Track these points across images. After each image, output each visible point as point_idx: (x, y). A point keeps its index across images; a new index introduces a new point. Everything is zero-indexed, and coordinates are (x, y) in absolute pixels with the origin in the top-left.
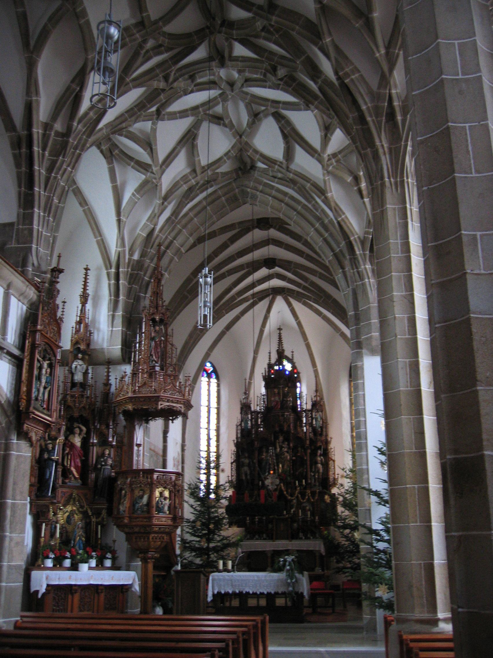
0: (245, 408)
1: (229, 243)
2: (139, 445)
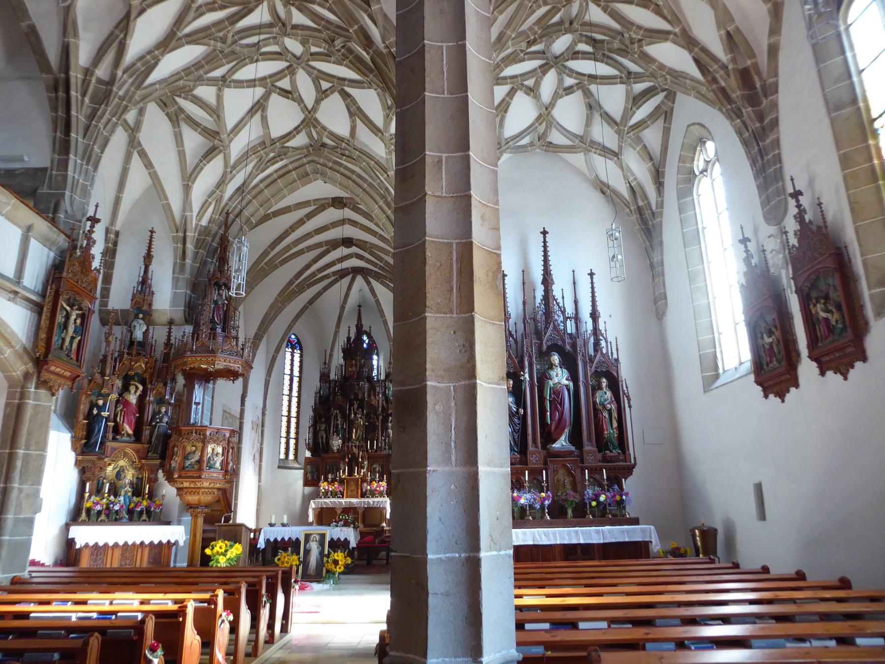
0: (324, 377)
1: (305, 219)
2: (197, 404)
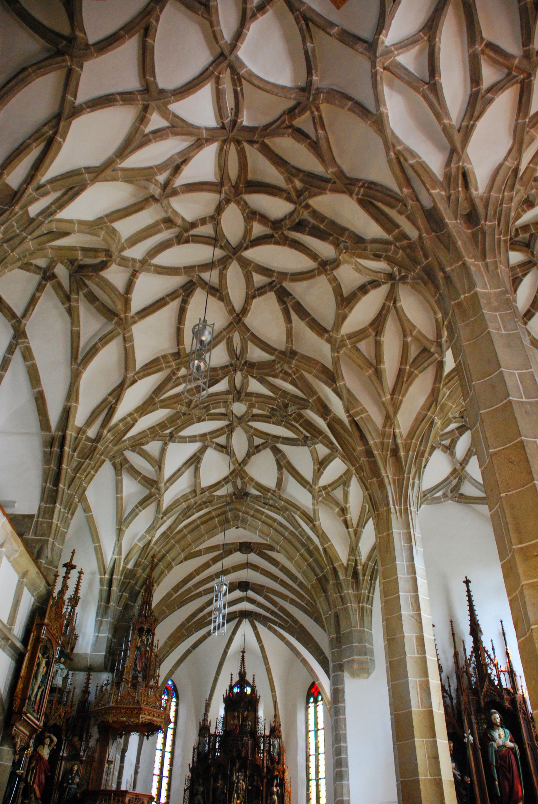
0: (204, 729)
1: (211, 563)
